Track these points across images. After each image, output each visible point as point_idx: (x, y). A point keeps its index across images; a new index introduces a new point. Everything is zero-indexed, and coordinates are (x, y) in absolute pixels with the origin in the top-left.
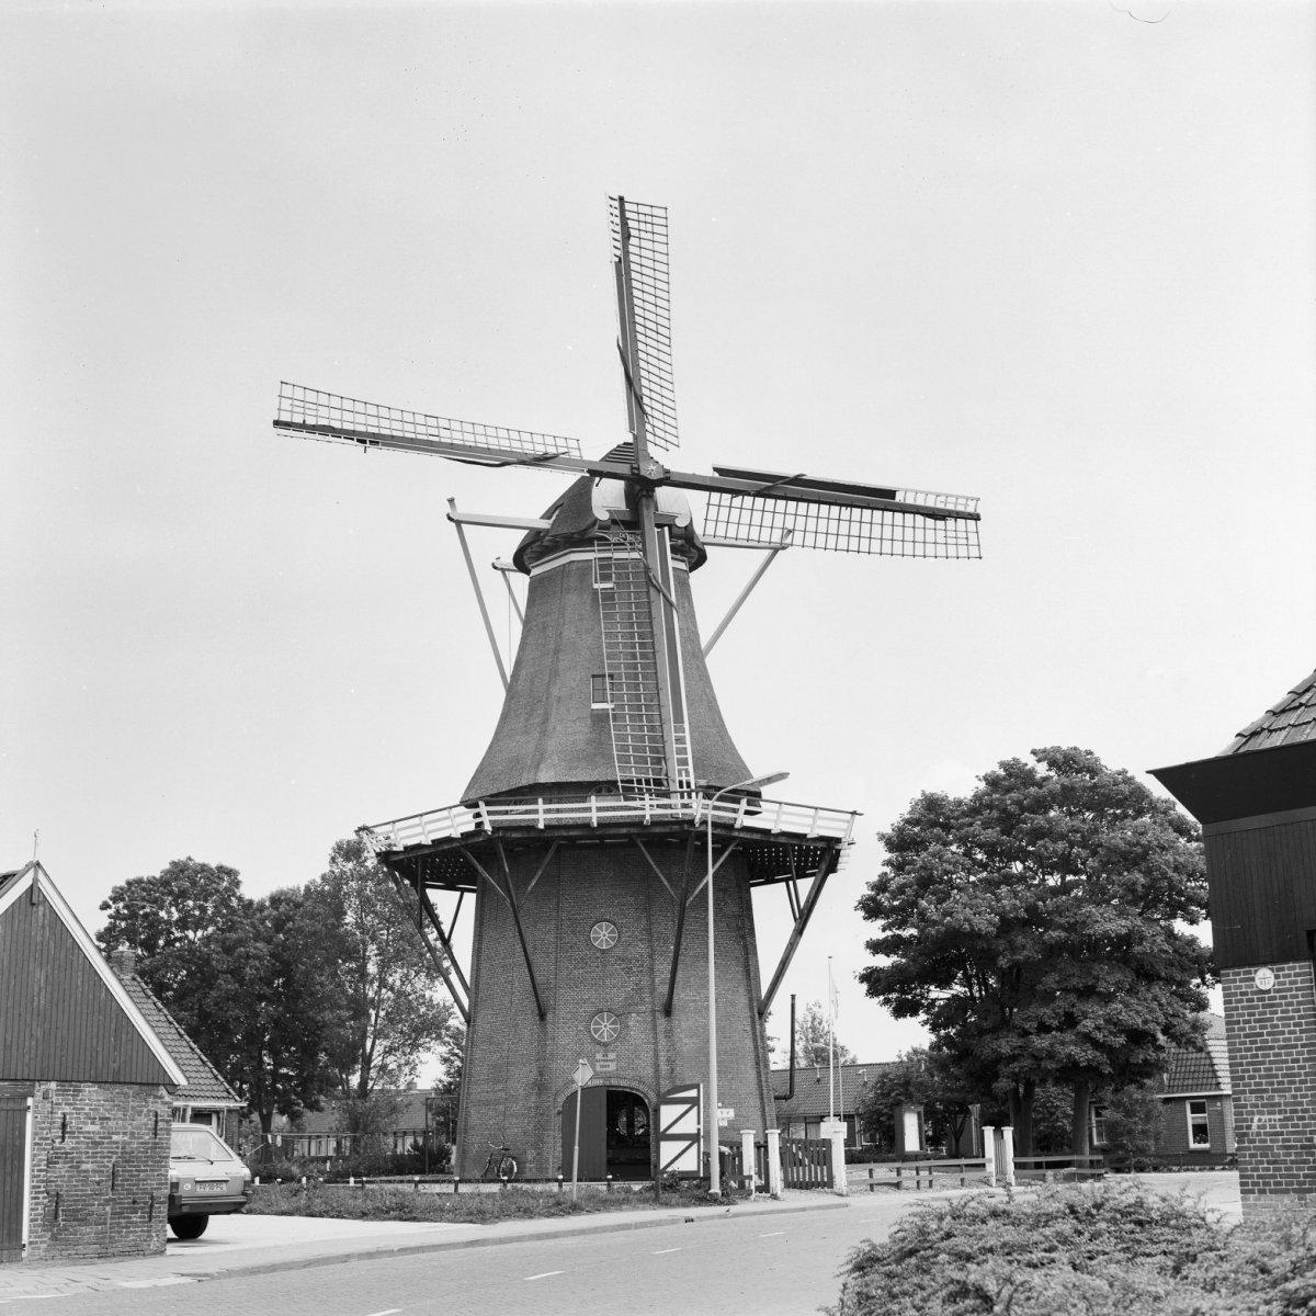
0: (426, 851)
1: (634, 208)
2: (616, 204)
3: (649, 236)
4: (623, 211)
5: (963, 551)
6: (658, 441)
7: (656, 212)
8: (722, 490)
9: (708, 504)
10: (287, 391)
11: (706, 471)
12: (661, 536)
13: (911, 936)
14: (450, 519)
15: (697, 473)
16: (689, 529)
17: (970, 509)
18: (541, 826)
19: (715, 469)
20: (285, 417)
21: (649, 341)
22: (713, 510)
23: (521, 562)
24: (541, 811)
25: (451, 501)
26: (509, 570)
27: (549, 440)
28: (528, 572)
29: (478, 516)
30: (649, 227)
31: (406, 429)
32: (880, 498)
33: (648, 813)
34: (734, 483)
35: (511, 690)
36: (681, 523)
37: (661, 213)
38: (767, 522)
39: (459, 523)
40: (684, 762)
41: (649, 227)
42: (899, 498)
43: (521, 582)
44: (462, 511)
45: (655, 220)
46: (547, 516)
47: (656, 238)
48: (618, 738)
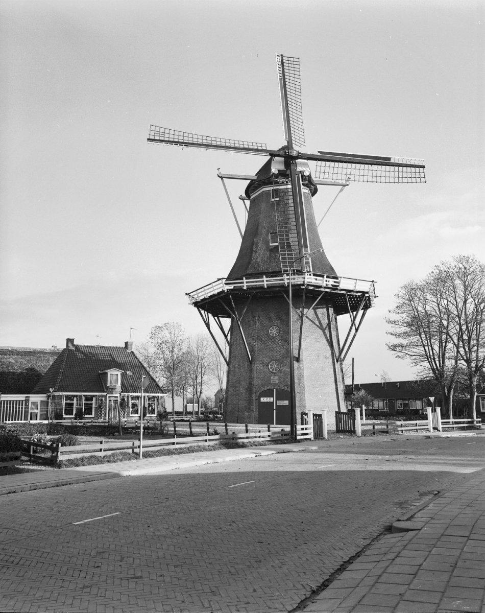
0: (207, 301)
1: (287, 59)
3: (293, 69)
5: (418, 180)
6: (297, 143)
7: (295, 60)
8: (324, 160)
9: (385, 183)
10: (153, 128)
11: (315, 152)
14: (219, 176)
15: (312, 153)
16: (309, 176)
18: (245, 288)
19: (319, 152)
20: (152, 137)
21: (293, 107)
22: (319, 168)
23: (248, 191)
24: (245, 282)
26: (245, 199)
27: (241, 143)
29: (235, 175)
30: (293, 66)
31: (170, 137)
32: (384, 162)
37: (297, 60)
38: (327, 171)
39: (222, 178)
41: (293, 66)
43: (248, 202)
44: (224, 172)
45: (295, 63)
47: (295, 69)
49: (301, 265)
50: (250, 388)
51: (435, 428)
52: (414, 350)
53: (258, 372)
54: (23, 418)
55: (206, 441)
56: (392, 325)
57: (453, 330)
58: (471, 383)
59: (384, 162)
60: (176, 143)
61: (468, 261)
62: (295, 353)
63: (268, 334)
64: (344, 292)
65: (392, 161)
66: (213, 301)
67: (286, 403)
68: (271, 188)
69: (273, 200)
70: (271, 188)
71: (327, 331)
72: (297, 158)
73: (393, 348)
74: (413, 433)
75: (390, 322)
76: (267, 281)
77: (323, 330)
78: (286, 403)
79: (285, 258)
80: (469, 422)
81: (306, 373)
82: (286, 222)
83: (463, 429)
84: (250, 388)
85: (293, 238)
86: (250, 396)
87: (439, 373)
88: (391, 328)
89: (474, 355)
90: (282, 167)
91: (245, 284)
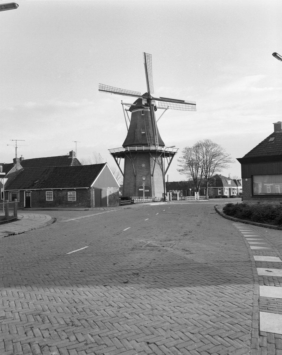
2: (144, 54)
4: (145, 54)
12: (153, 107)
13: (71, 164)
14: (121, 104)
16: (156, 106)
17: (195, 104)
23: (130, 110)
25: (122, 101)
28: (131, 112)
30: (149, 58)
32: (182, 102)
33: (144, 149)
34: (162, 99)
35: (129, 131)
36: (155, 105)
37: (150, 55)
39: (123, 104)
40: (157, 141)
42: (185, 102)
43: (130, 113)
44: (123, 102)
46: (134, 103)
48: (147, 136)
49: (155, 142)
50: (135, 186)
51: (197, 199)
52: (187, 172)
53: (138, 180)
54: (142, 197)
55: (192, 199)
56: (180, 162)
57: (201, 164)
58: (207, 184)
59: (182, 102)
60: (110, 92)
61: (208, 141)
62: (152, 173)
63: (141, 167)
64: (169, 152)
65: (185, 102)
66: (122, 153)
67: (148, 191)
68: (142, 110)
69: (142, 115)
70: (142, 110)
71: (161, 165)
72: (152, 99)
73: (180, 171)
74: (191, 200)
75: (178, 161)
76: (144, 148)
77: (160, 165)
78: (148, 191)
79: (151, 139)
80: (205, 197)
81: (155, 180)
82: (148, 125)
83: (204, 199)
84: (135, 186)
85: (151, 131)
86: (135, 189)
87: (195, 180)
88: (179, 163)
89: (208, 174)
90: (146, 102)
91: (136, 149)
